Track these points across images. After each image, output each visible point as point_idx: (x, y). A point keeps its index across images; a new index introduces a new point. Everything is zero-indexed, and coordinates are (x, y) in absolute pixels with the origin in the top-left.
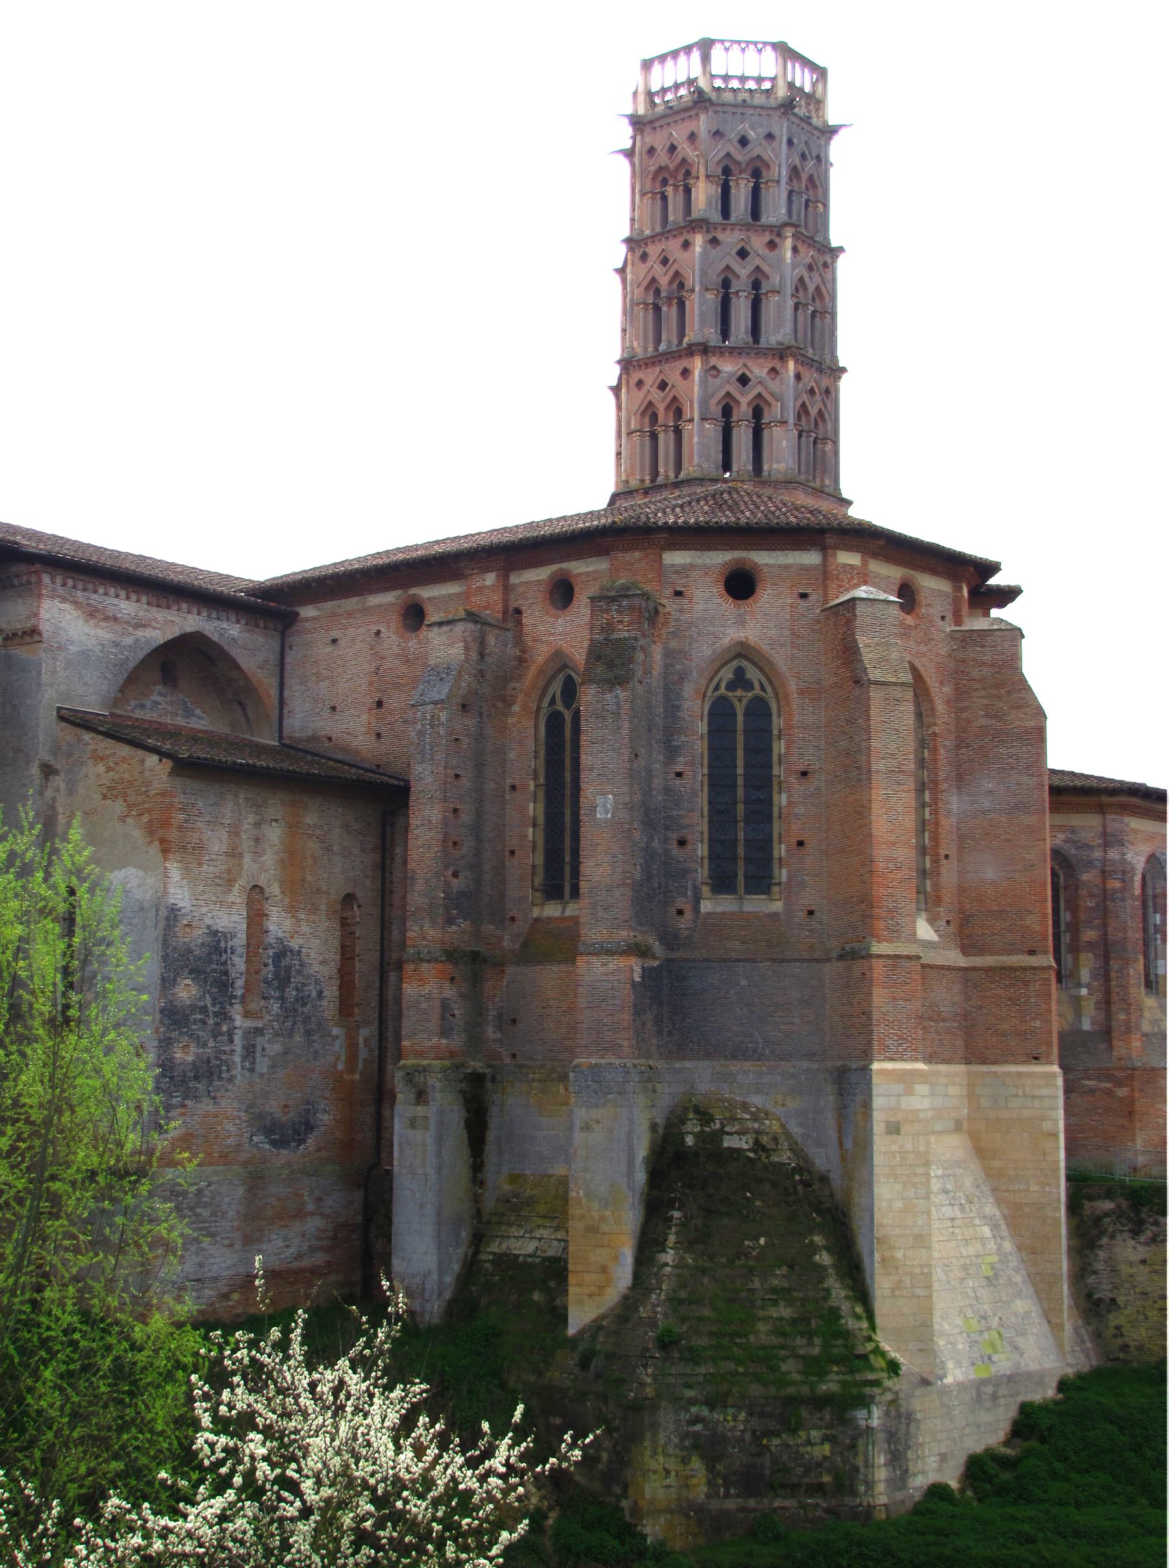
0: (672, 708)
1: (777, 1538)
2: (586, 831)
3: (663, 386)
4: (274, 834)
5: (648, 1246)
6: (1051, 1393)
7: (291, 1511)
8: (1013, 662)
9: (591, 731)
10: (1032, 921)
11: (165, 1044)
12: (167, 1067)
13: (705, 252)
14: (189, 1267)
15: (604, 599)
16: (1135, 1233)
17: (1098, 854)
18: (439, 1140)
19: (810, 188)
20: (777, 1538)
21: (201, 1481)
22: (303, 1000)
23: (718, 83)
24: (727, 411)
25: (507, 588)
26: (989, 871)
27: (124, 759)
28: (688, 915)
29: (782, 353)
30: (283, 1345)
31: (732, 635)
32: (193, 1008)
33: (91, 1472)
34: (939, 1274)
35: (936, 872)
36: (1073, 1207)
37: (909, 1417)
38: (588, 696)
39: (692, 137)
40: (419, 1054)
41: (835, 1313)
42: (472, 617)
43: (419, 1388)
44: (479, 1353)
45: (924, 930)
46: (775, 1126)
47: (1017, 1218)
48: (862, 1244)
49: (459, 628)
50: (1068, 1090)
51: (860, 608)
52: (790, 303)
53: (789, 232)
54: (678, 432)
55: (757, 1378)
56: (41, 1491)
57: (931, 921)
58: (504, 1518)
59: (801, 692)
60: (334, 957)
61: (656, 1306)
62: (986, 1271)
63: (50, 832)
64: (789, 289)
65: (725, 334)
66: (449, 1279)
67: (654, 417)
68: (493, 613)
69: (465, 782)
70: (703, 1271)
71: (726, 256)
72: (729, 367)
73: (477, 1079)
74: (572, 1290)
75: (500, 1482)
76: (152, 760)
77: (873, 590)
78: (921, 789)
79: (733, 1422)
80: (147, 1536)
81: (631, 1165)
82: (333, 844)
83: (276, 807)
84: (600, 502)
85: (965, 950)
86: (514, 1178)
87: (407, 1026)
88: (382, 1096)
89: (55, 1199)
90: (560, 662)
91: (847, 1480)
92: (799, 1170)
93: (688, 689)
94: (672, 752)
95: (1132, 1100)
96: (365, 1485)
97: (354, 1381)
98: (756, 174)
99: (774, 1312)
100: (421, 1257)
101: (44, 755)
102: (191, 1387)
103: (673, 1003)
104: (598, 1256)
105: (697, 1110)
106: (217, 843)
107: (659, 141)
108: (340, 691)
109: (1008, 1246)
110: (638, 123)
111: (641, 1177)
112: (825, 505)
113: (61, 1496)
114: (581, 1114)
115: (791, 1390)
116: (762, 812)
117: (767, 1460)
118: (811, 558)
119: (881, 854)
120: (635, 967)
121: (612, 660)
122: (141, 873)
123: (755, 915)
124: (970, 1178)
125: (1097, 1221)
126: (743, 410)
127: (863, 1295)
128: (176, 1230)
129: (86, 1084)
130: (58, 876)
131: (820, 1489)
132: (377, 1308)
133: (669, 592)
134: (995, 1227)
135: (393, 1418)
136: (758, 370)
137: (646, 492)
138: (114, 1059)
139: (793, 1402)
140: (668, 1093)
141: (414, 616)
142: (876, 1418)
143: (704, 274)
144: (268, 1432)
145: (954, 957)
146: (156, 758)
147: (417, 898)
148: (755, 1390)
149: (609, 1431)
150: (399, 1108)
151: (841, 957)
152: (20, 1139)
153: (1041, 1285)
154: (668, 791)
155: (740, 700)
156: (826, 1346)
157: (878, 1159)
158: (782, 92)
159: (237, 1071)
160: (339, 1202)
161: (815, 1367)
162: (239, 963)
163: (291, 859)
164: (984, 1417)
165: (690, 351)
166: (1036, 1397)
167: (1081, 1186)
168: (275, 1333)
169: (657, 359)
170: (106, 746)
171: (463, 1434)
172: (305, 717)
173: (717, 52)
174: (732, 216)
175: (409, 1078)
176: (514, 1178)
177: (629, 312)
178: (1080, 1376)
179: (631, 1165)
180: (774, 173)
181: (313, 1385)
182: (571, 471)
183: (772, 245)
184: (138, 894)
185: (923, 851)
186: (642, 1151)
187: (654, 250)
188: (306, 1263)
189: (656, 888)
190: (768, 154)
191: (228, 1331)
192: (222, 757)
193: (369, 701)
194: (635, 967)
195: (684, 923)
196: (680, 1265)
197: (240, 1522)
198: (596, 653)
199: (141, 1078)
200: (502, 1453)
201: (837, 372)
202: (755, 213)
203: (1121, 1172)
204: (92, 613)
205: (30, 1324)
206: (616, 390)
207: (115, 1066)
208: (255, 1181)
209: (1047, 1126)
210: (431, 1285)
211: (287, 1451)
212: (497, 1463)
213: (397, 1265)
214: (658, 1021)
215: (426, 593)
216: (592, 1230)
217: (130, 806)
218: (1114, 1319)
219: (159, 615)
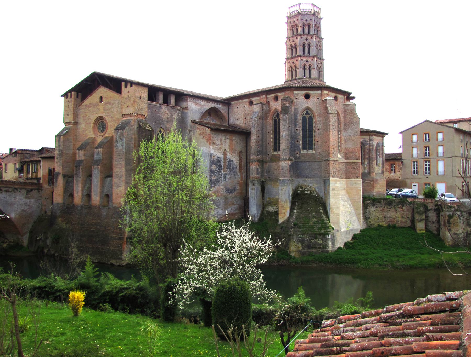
0: (296, 118)
1: (313, 255)
2: (281, 139)
3: (293, 63)
4: (228, 141)
5: (292, 209)
6: (359, 232)
7: (234, 251)
8: (354, 110)
9: (282, 123)
10: (357, 154)
11: (211, 176)
12: (211, 180)
13: (300, 40)
14: (216, 213)
15: (284, 99)
16: (373, 206)
17: (368, 143)
18: (257, 192)
19: (318, 28)
20: (313, 255)
21: (219, 246)
22: (233, 169)
23: (302, 11)
24: (304, 67)
25: (267, 98)
26: (350, 146)
28: (299, 153)
29: (314, 57)
30: (231, 225)
31: (306, 105)
32: (215, 170)
33: (201, 244)
34: (341, 213)
35: (341, 146)
36: (363, 202)
37: (335, 236)
38: (281, 116)
39: (298, 20)
40: (253, 178)
41: (323, 220)
42: (261, 103)
43: (254, 232)
44: (264, 226)
45: (339, 156)
46: (313, 189)
47: (354, 204)
48: (328, 209)
49: (259, 105)
50: (363, 183)
51: (328, 100)
52: (315, 48)
53: (315, 36)
54: (296, 70)
55: (310, 231)
56: (193, 248)
57: (340, 154)
58: (268, 253)
59: (318, 115)
60: (238, 161)
61: (293, 219)
62: (348, 213)
63: (190, 140)
64: (315, 45)
65: (304, 53)
66: (259, 215)
67: (292, 68)
68: (264, 102)
69: (260, 131)
70: (301, 213)
71: (304, 40)
72: (305, 59)
73: (263, 182)
74: (279, 217)
77: (330, 97)
78: (338, 131)
79: (306, 238)
80: (211, 254)
81: (289, 196)
82: (238, 144)
83: (228, 136)
84: (283, 83)
85: (346, 159)
86: (269, 198)
87: (251, 173)
88: (247, 185)
89: (193, 202)
90: (276, 111)
91: (325, 246)
92: (317, 196)
93: (298, 115)
94: (296, 126)
95: (373, 184)
96: (245, 247)
97: (243, 231)
98: (309, 26)
99: (313, 220)
100: (254, 211)
101: (189, 128)
102: (217, 232)
103: (296, 169)
104: (283, 211)
105: (300, 187)
106: (218, 142)
107: (292, 21)
108: (239, 116)
109: (352, 209)
110: (288, 18)
111: (291, 198)
112: (321, 83)
113: (197, 248)
114: (280, 188)
115: (316, 232)
116: (311, 136)
117: (312, 243)
118: (319, 92)
119: (331, 143)
120: (289, 162)
121: (285, 110)
123: (310, 154)
124: (346, 198)
125: (367, 204)
126: (307, 67)
127: (328, 217)
128: (213, 207)
129: (197, 183)
130: (191, 148)
131: (320, 248)
132: (247, 219)
133: (295, 98)
134: (350, 205)
135: (250, 237)
136: (310, 59)
137: (291, 81)
138: (202, 178)
139: (316, 234)
140: (295, 184)
141: (251, 103)
142: (330, 237)
143: (300, 43)
144: (229, 239)
145: (344, 161)
147: (252, 151)
148: (310, 233)
149: (285, 239)
150: (250, 187)
151: (325, 161)
152: (187, 191)
153: (358, 215)
154: (295, 132)
155: (307, 116)
156: (322, 225)
157: (331, 194)
158: (313, 12)
159: (223, 181)
160: (240, 202)
161: (320, 229)
162: (222, 163)
163: (231, 145)
164: (348, 236)
165: (298, 56)
166: (356, 233)
167: (364, 198)
168: (230, 223)
169: (292, 58)
170: (199, 126)
171: (261, 239)
172: (233, 121)
173: (301, 5)
174: (305, 33)
175: (252, 181)
176: (269, 198)
177: (287, 50)
178: (363, 229)
179: (289, 196)
180: (312, 26)
181: (236, 232)
182: (278, 78)
183: (312, 38)
184: (205, 151)
185: (339, 142)
186: (291, 194)
187: (291, 39)
188: (235, 212)
189: (293, 149)
190: (311, 23)
191: (222, 223)
192: (219, 128)
193: (244, 118)
194: (289, 162)
195: (298, 155)
196: (297, 212)
197: (225, 253)
198: (282, 109)
199: (206, 182)
200: (268, 242)
201: (323, 60)
202: (309, 32)
203: (371, 196)
204: (197, 104)
205: (190, 222)
206: (285, 63)
207: (202, 180)
208: (226, 199)
209: (359, 189)
210: (256, 216)
211: (232, 242)
212: (267, 244)
213: (250, 212)
214: (293, 172)
215: (253, 99)
216: (283, 207)
218: (369, 220)
219: (208, 104)
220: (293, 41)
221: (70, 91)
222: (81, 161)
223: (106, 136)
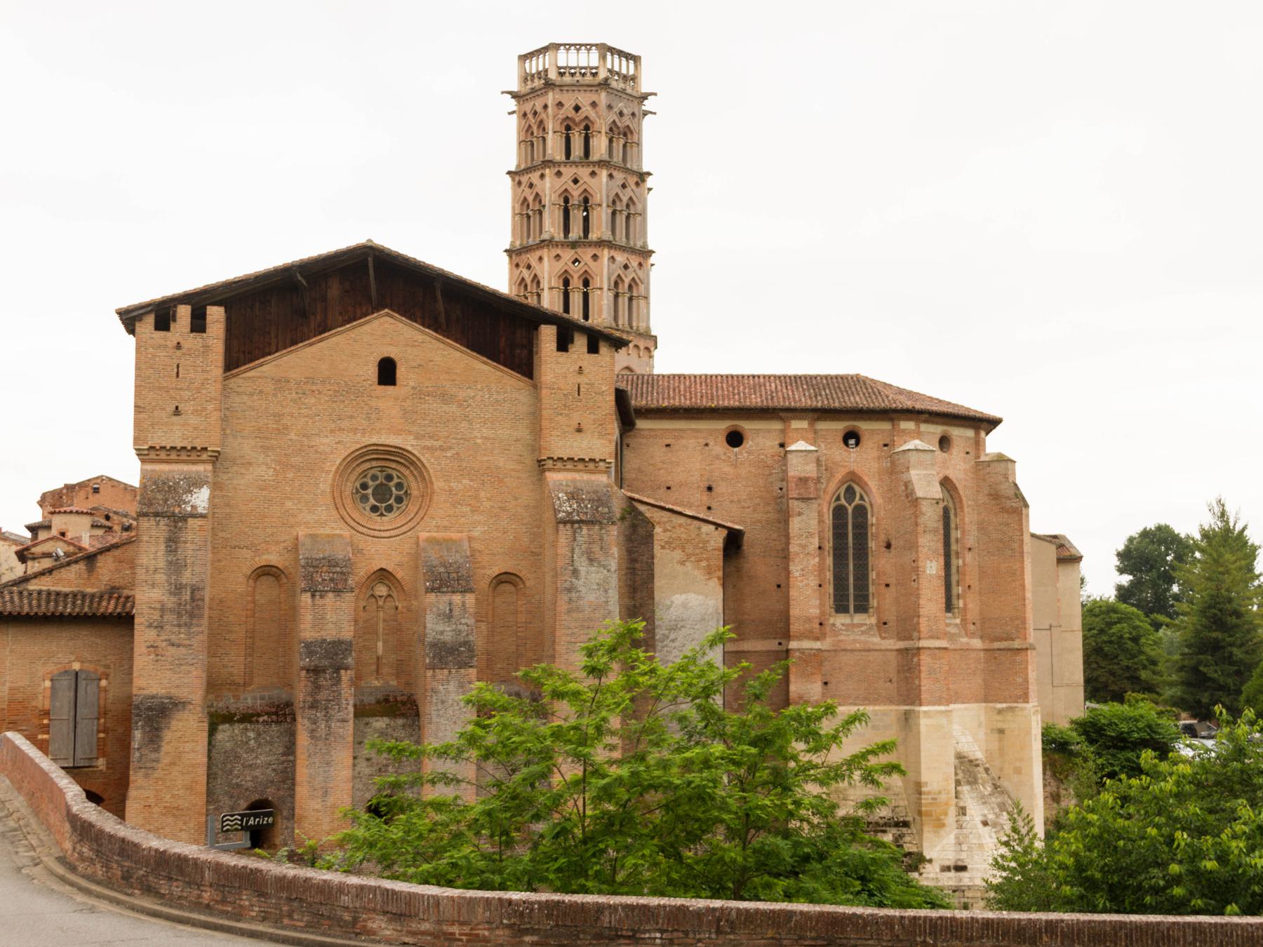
19: (625, 134)
24: (566, 283)
27: (680, 525)
39: (594, 104)
146: (712, 527)
180: (596, 127)
183: (593, 174)
187: (524, 179)
190: (592, 115)
202: (587, 153)
217: (689, 556)
220: (576, 181)
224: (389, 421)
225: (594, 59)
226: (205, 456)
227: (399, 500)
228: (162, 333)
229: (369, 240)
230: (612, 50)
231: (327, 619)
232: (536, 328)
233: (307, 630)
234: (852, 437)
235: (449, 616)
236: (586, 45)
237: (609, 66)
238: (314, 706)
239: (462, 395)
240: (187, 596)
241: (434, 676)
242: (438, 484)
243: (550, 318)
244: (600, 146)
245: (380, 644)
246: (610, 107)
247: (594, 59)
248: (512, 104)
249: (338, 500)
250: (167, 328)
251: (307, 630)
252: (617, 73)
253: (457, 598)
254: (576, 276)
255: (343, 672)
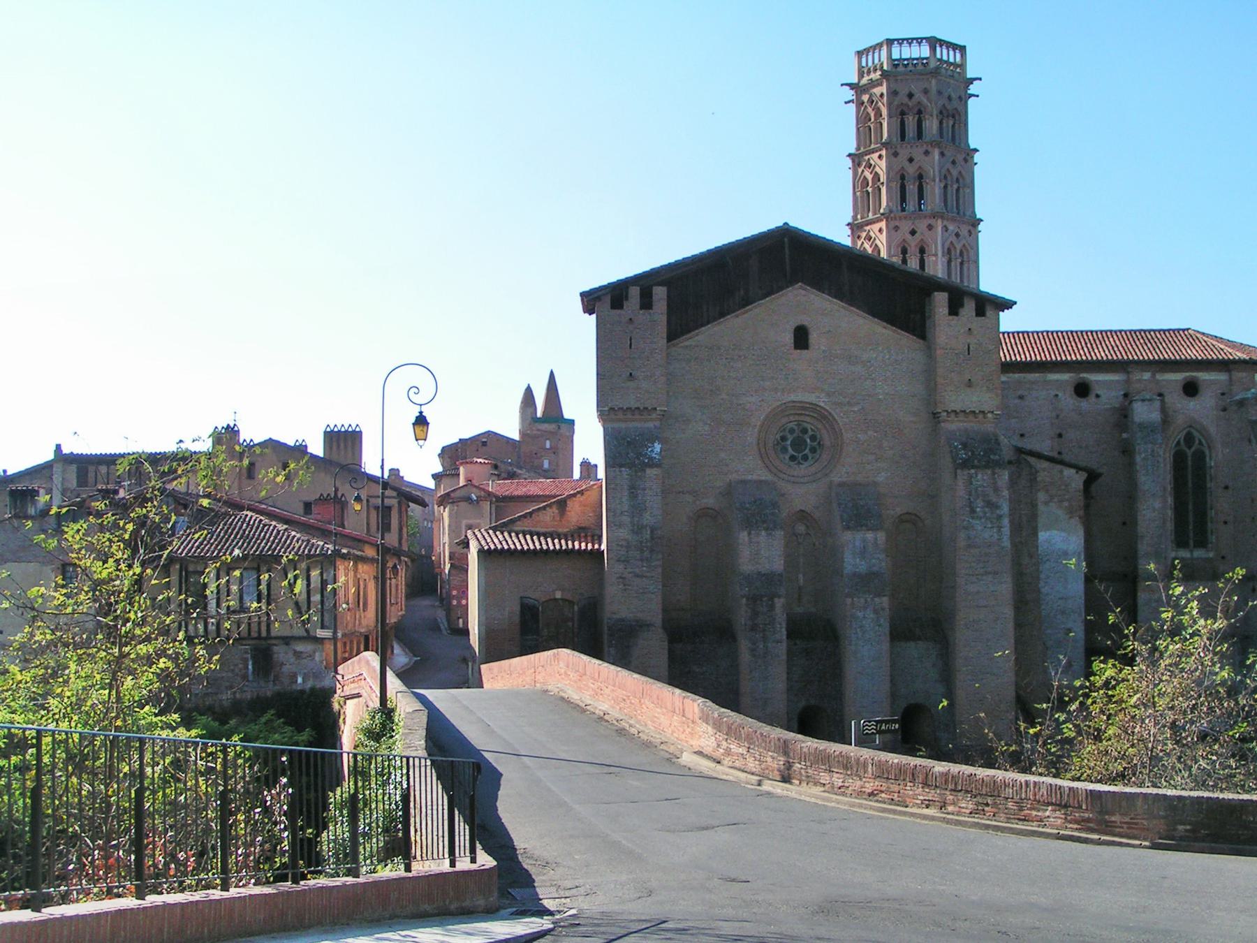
19: (955, 118)
39: (926, 92)
75: (82, 525)
76: (1069, 472)
122: (1063, 534)
141: (1082, 390)
146: (1073, 471)
183: (927, 153)
220: (911, 160)
221: (645, 283)
222: (770, 579)
223: (836, 478)
224: (805, 382)
225: (925, 51)
226: (654, 416)
227: (813, 450)
228: (618, 311)
229: (786, 224)
230: (942, 43)
231: (762, 553)
232: (929, 294)
233: (746, 564)
234: (1191, 389)
235: (863, 553)
236: (897, 40)
237: (938, 56)
238: (753, 628)
239: (865, 357)
240: (647, 534)
241: (853, 603)
242: (847, 436)
243: (938, 286)
244: (931, 126)
245: (801, 576)
246: (940, 93)
247: (925, 51)
248: (849, 94)
249: (763, 450)
250: (621, 307)
251: (746, 564)
252: (952, 64)
253: (870, 535)
254: (913, 244)
255: (776, 600)
